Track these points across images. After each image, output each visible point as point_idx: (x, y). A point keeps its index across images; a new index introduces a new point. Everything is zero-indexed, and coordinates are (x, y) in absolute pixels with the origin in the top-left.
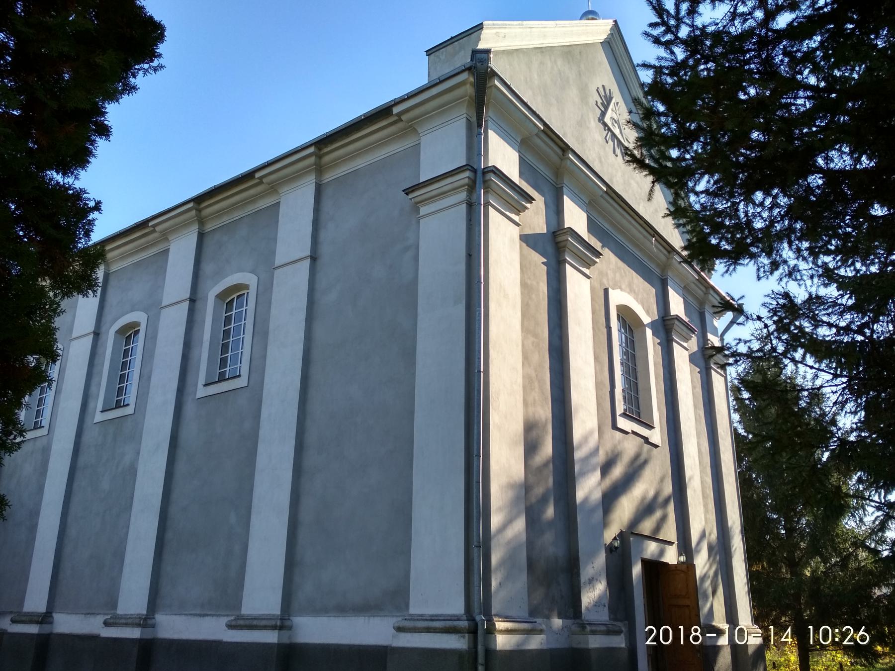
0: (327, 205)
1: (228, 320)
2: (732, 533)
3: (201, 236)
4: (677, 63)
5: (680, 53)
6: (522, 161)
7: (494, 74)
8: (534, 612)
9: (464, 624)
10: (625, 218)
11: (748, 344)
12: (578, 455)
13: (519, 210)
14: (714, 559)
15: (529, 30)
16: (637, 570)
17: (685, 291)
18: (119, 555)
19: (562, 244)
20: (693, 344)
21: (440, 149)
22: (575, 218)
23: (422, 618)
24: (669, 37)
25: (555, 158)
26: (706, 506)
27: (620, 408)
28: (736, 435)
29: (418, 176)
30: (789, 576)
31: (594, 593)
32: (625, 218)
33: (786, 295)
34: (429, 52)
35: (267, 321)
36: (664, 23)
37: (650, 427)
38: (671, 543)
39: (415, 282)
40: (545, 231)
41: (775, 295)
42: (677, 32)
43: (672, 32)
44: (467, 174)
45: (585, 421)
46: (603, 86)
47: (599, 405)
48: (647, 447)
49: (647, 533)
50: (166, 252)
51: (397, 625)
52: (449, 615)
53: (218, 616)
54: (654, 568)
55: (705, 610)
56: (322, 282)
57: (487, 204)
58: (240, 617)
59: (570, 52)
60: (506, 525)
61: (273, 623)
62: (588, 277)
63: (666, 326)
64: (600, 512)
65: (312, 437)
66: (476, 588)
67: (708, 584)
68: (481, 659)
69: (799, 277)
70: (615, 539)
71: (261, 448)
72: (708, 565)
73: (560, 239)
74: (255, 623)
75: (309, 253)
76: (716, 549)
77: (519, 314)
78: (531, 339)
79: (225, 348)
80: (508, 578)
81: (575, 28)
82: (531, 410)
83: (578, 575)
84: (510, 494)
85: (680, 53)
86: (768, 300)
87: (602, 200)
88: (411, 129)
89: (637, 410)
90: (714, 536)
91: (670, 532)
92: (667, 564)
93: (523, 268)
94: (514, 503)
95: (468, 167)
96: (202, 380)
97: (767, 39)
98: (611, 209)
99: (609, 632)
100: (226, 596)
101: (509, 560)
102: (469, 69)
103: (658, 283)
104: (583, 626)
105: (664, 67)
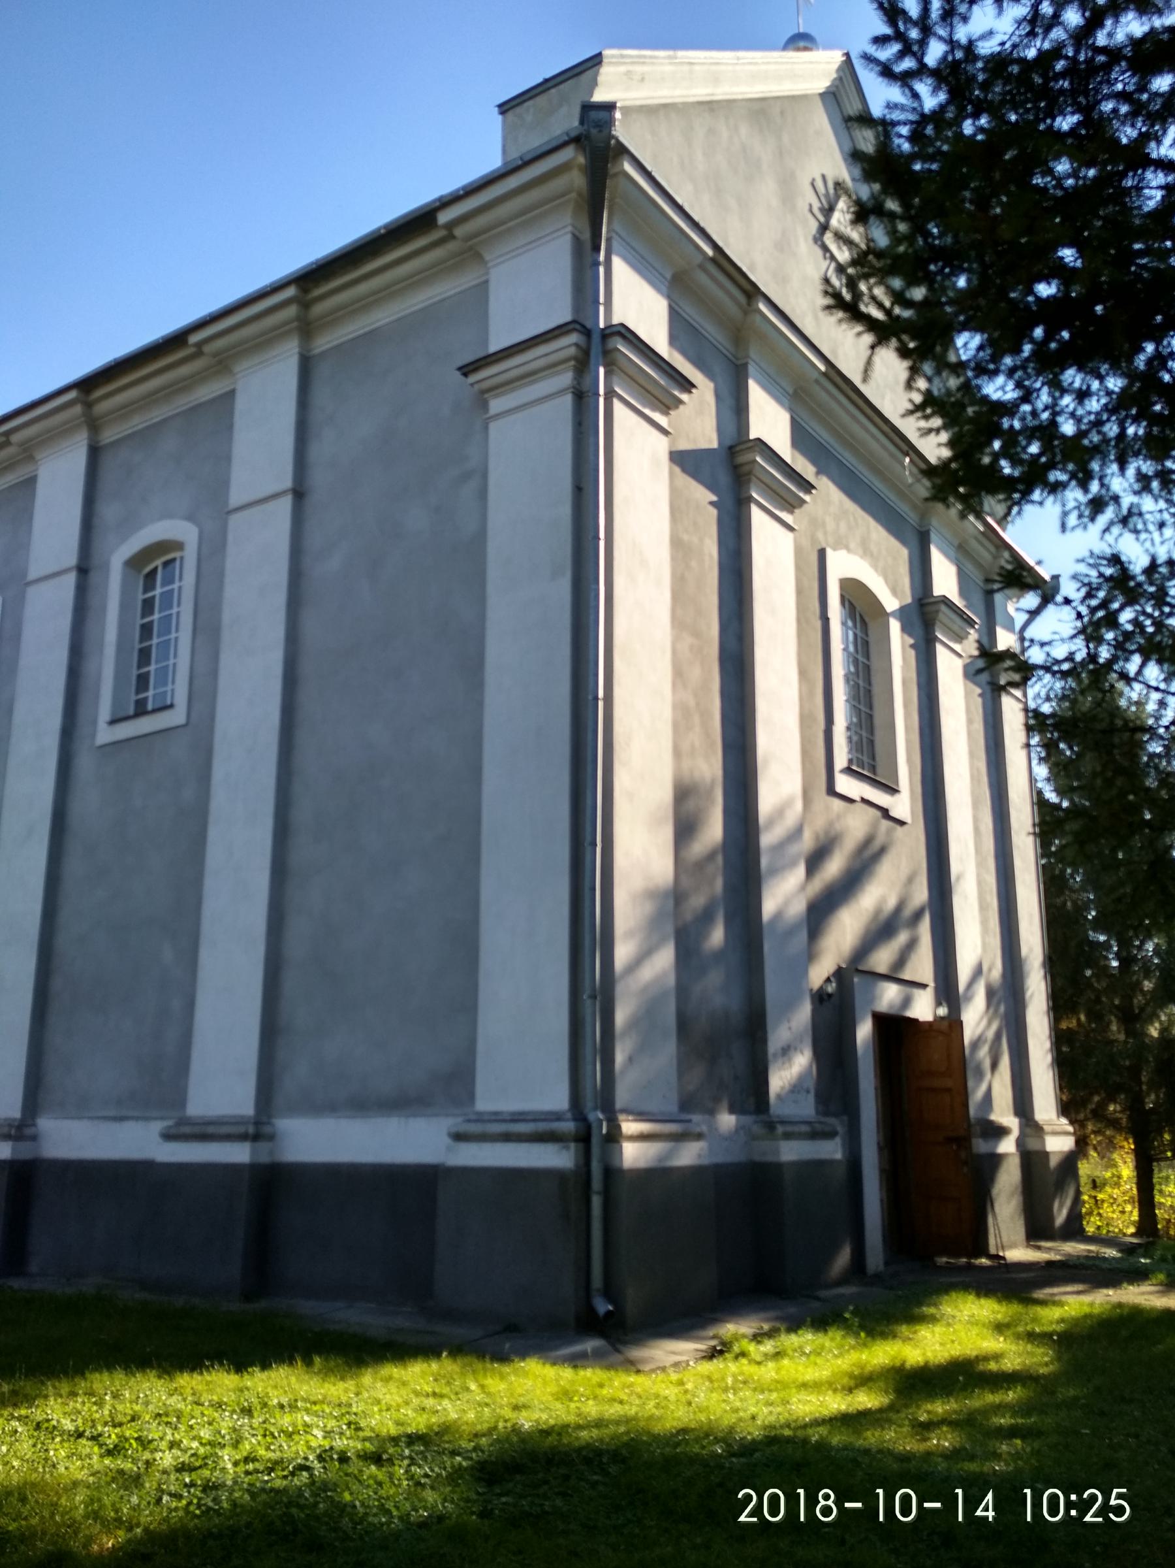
0: (322, 396)
1: (148, 606)
2: (1027, 968)
3: (95, 453)
4: (923, 115)
5: (931, 98)
6: (674, 315)
8: (687, 1104)
9: (568, 1126)
10: (858, 422)
11: (1046, 648)
12: (767, 840)
13: (668, 405)
14: (996, 1011)
15: (686, 68)
16: (864, 1031)
17: (961, 554)
19: (746, 469)
20: (969, 647)
21: (524, 291)
22: (770, 421)
23: (496, 1117)
24: (908, 64)
25: (734, 311)
26: (984, 922)
27: (841, 758)
28: (1040, 802)
29: (485, 342)
30: (1122, 1037)
31: (790, 1071)
32: (858, 422)
33: (1115, 560)
34: (505, 108)
35: (216, 606)
36: (899, 36)
38: (924, 986)
39: (481, 536)
40: (715, 445)
41: (1095, 559)
42: (923, 54)
43: (914, 54)
44: (574, 338)
45: (780, 783)
46: (824, 177)
47: (806, 753)
48: (885, 824)
49: (882, 968)
50: (31, 481)
51: (454, 1130)
52: (542, 1113)
53: (147, 1119)
54: (894, 1029)
55: (978, 1094)
56: (315, 538)
57: (610, 394)
58: (184, 1121)
59: (763, 112)
60: (642, 963)
61: (241, 1129)
62: (790, 528)
63: (925, 615)
64: (803, 935)
65: (303, 813)
66: (589, 1068)
67: (983, 1053)
68: (597, 1183)
69: (1140, 526)
70: (828, 980)
71: (213, 833)
72: (984, 1022)
73: (741, 459)
74: (211, 1130)
76: (1000, 994)
77: (667, 595)
78: (688, 640)
79: (144, 656)
80: (642, 1049)
81: (772, 67)
82: (686, 764)
83: (764, 1041)
84: (648, 908)
85: (931, 98)
86: (1082, 568)
87: (817, 388)
88: (472, 254)
89: (871, 762)
90: (996, 972)
91: (922, 966)
92: (916, 1021)
93: (676, 512)
94: (654, 923)
95: (580, 325)
96: (105, 712)
97: (1087, 72)
98: (834, 405)
99: (816, 1135)
100: (160, 1084)
101: (646, 1017)
102: (576, 140)
103: (914, 541)
104: (770, 1126)
105: (898, 123)
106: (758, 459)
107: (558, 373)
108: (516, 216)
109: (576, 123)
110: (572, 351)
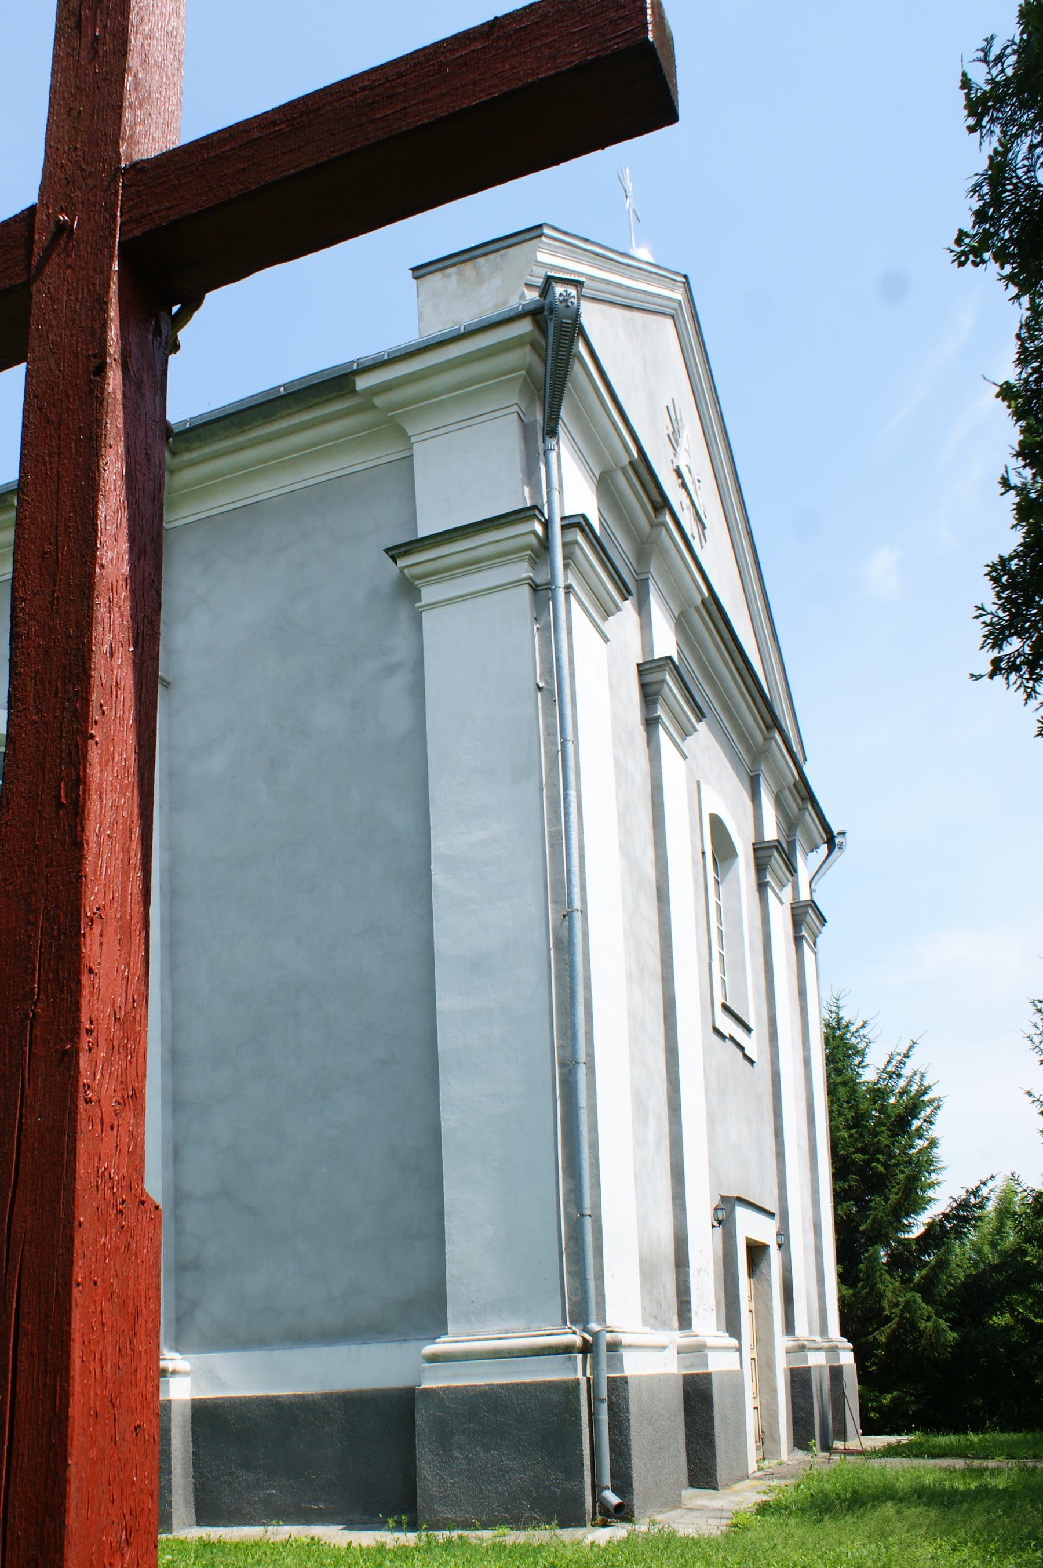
7: (582, 332)
21: (463, 471)
106: (668, 678)
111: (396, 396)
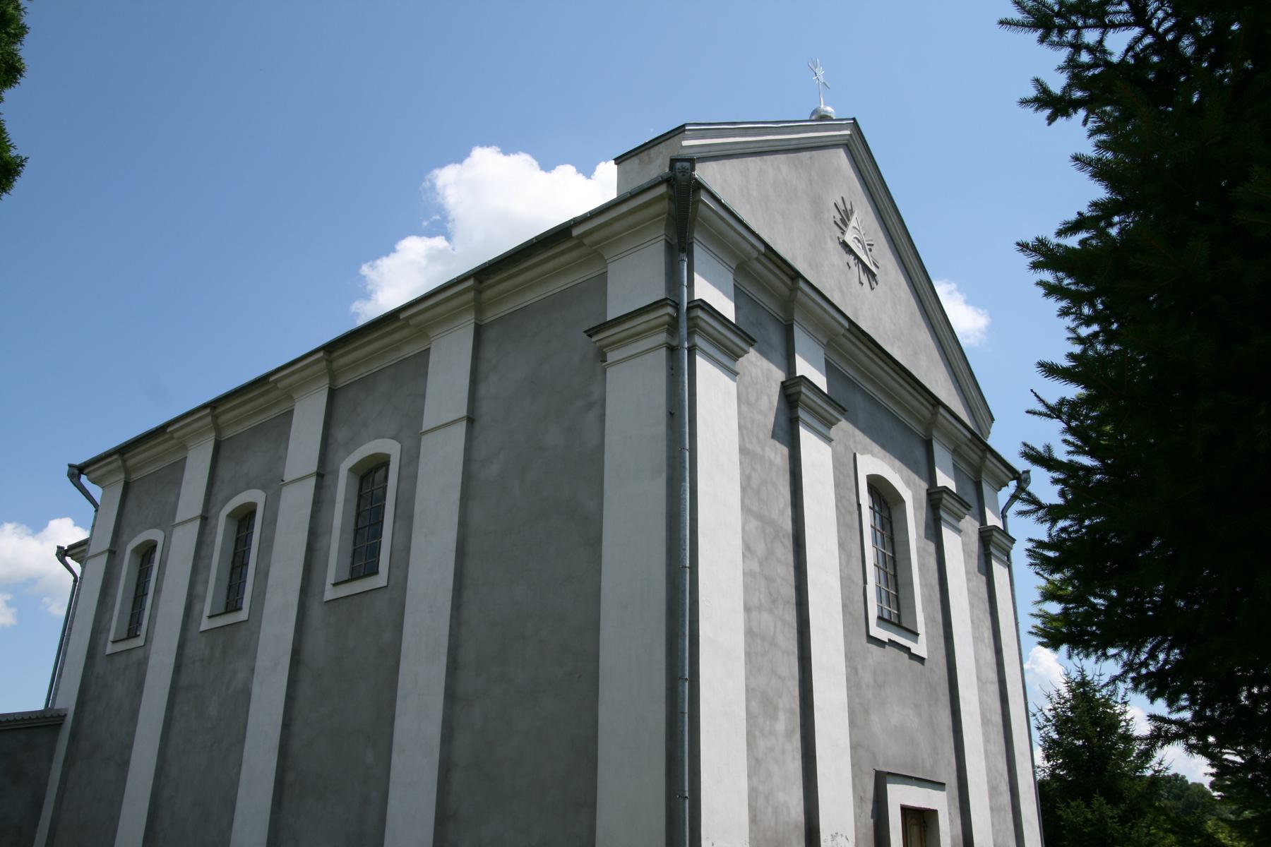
0: (489, 352)
18: (230, 801)
21: (634, 280)
25: (783, 289)
37: (914, 634)
57: (692, 350)
75: (464, 413)
107: (657, 334)
108: (627, 230)
109: (667, 170)
110: (666, 318)
111: (596, 237)
